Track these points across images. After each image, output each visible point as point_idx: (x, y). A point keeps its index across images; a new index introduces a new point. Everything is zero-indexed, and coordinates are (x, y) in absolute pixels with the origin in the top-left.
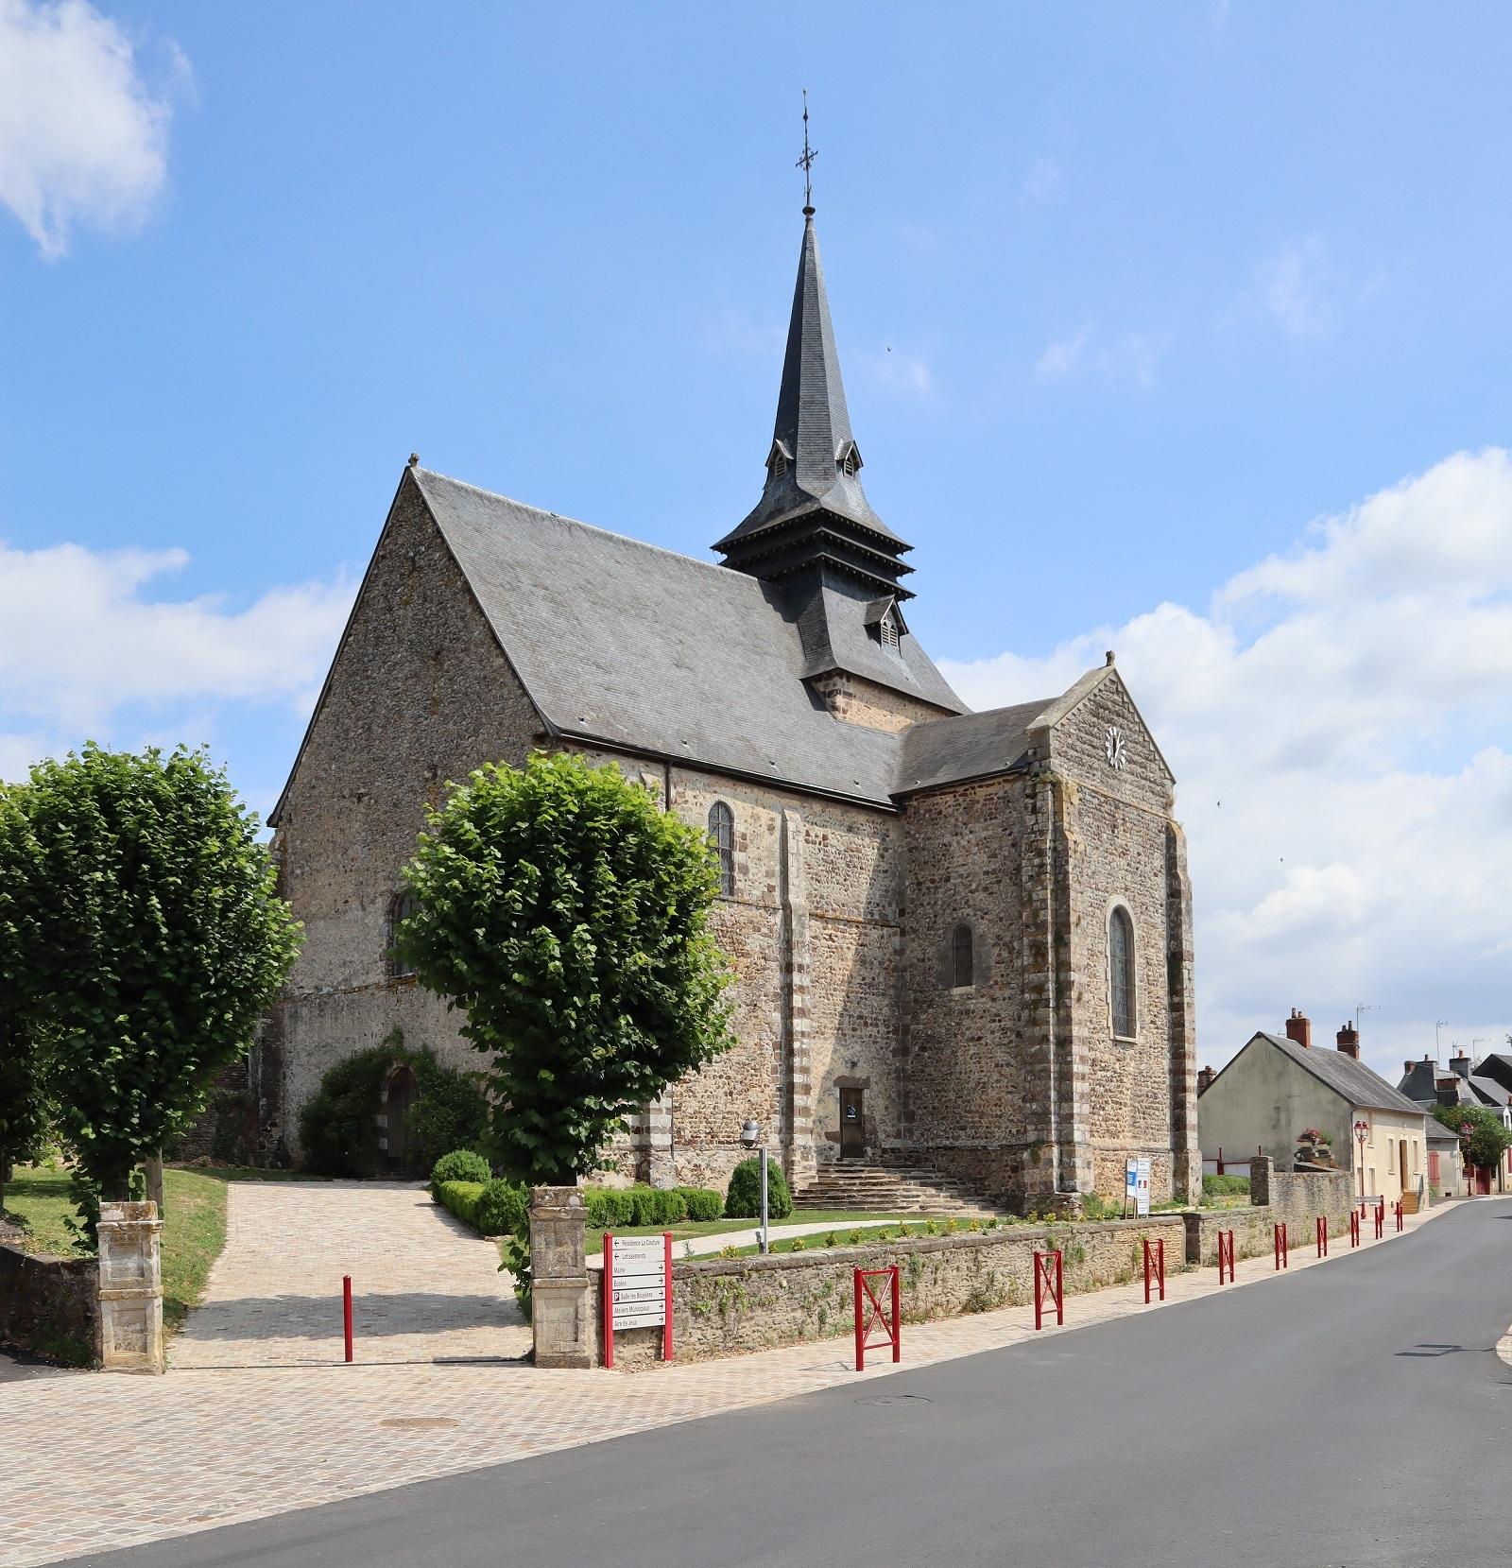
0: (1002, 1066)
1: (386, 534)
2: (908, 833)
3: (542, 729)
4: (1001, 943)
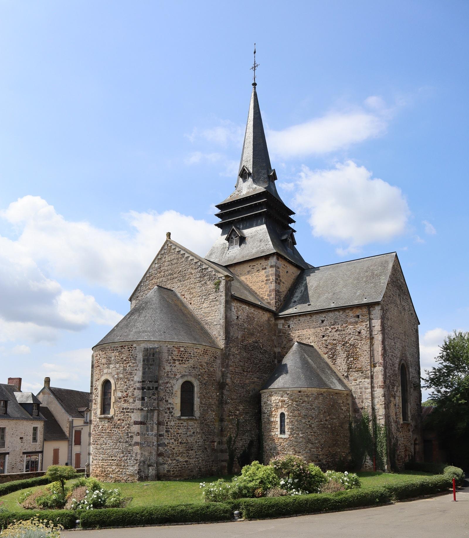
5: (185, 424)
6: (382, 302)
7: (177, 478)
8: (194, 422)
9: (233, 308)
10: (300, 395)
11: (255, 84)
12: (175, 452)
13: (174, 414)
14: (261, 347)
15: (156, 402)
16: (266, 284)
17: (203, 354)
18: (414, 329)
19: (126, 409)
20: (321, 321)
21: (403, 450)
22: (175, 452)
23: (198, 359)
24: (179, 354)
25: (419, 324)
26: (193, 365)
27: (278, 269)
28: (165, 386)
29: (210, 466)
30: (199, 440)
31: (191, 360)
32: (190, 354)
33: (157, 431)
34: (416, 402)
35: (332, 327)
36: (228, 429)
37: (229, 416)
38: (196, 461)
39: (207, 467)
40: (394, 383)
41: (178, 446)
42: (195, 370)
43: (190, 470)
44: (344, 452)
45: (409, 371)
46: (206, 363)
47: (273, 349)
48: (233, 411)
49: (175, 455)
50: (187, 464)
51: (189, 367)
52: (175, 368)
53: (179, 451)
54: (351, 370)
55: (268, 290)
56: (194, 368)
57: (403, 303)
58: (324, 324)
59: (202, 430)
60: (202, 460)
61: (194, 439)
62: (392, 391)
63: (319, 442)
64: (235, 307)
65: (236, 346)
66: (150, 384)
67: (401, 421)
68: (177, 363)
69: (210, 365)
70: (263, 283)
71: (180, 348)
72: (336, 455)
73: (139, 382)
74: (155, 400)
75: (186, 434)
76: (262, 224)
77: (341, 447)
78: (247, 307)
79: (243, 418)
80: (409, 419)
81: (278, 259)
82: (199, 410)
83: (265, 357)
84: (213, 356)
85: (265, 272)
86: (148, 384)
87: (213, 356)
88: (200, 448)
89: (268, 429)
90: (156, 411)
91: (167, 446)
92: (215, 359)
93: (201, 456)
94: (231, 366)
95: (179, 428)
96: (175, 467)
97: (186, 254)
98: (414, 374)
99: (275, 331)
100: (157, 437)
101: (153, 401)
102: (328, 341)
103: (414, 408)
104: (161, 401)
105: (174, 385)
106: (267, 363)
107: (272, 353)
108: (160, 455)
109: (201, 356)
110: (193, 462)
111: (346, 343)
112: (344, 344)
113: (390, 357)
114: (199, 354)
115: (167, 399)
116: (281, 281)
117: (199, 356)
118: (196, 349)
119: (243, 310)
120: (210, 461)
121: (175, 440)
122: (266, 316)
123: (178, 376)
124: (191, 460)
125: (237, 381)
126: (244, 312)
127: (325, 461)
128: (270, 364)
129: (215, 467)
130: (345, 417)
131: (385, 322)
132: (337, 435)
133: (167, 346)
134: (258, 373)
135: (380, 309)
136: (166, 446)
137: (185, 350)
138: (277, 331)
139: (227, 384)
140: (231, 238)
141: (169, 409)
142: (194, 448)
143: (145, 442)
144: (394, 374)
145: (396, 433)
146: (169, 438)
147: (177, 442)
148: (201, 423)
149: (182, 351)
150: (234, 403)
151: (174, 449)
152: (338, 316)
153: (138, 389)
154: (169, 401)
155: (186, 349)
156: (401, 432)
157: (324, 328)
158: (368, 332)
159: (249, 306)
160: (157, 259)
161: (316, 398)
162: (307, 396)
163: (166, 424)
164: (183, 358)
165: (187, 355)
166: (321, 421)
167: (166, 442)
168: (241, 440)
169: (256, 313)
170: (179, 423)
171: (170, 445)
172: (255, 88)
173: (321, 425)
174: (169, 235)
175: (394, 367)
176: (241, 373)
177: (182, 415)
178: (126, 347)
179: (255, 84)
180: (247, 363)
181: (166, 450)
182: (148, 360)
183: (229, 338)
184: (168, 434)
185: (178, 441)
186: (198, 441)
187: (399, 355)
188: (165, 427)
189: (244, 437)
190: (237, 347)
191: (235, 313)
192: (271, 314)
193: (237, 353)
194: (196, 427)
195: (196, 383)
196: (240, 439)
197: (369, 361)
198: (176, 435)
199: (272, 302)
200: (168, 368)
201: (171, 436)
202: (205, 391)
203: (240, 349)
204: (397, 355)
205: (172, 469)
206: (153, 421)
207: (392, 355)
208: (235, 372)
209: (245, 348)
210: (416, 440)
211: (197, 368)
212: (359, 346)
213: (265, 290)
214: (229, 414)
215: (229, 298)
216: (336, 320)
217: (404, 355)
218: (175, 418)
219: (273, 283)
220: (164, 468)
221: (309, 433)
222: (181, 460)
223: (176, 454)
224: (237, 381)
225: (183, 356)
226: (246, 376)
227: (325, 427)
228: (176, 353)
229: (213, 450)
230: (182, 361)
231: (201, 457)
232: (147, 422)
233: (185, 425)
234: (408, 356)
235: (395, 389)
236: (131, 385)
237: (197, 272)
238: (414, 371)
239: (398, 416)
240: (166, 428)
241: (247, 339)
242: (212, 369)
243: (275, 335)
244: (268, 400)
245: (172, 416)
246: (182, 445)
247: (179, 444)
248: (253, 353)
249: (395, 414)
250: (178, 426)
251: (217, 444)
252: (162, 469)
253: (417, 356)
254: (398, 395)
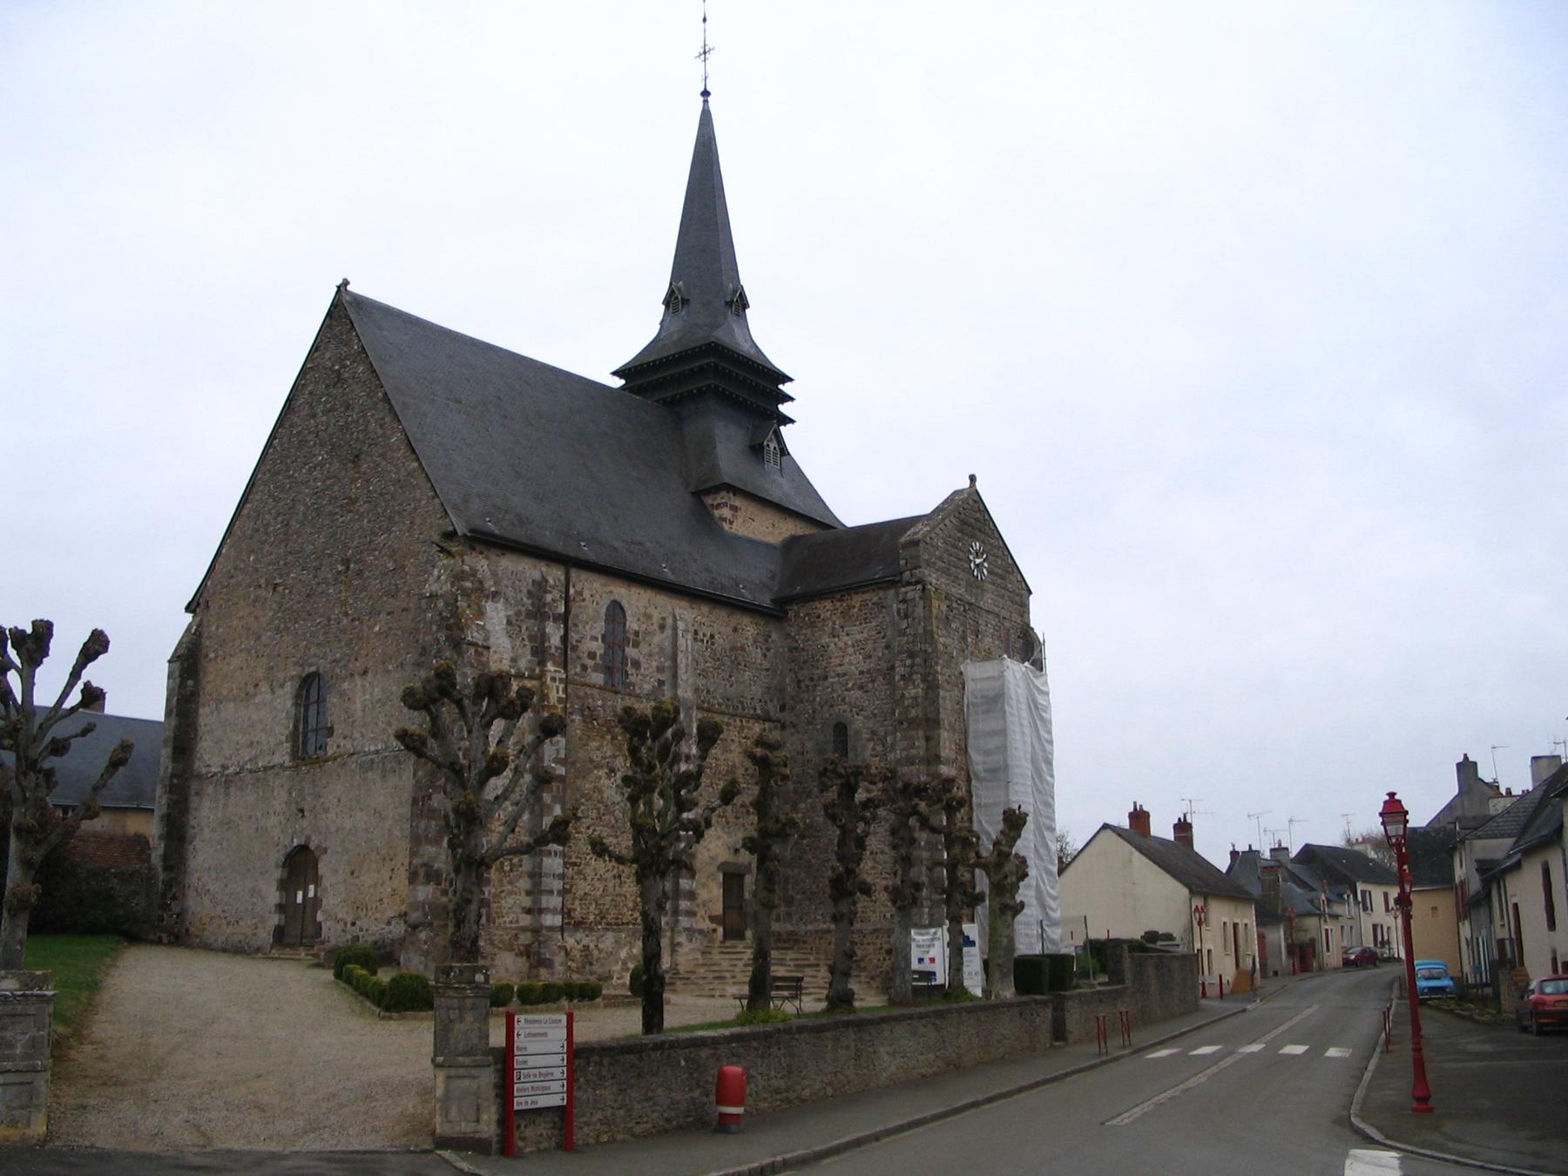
0: (877, 853)
1: (316, 347)
2: (789, 635)
3: (451, 529)
4: (875, 737)
11: (706, 93)
172: (706, 102)
179: (706, 93)
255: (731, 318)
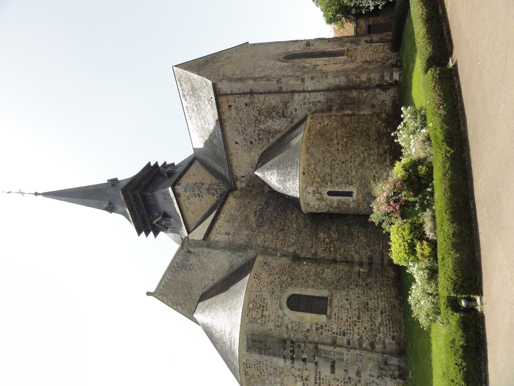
5: (336, 310)
6: (214, 81)
7: (402, 328)
8: (334, 297)
9: (216, 239)
10: (308, 173)
12: (370, 327)
13: (324, 323)
14: (261, 207)
15: (308, 345)
16: (202, 197)
17: (258, 279)
18: (251, 47)
19: (316, 380)
20: (237, 145)
21: (377, 54)
22: (370, 327)
23: (264, 287)
24: (257, 310)
25: (248, 43)
26: (270, 293)
27: (189, 185)
28: (291, 330)
29: (389, 281)
30: (355, 293)
31: (264, 295)
32: (257, 296)
33: (343, 347)
34: (326, 43)
35: (241, 133)
36: (346, 253)
37: (331, 252)
38: (382, 299)
39: (389, 285)
40: (301, 67)
41: (362, 322)
42: (275, 292)
43: (393, 308)
44: (377, 122)
45: (292, 52)
46: (269, 277)
47: (266, 194)
48: (325, 246)
49: (373, 327)
50: (386, 312)
51: (272, 299)
52: (271, 316)
53: (368, 321)
54: (285, 114)
55: (208, 195)
56: (273, 293)
57: (223, 59)
58: (239, 142)
59: (344, 288)
60: (381, 291)
61: (354, 299)
62: (309, 69)
63: (363, 152)
64: (215, 237)
65: (256, 238)
66: (287, 350)
67: (345, 57)
68: (265, 313)
69: (272, 271)
70: (202, 200)
71: (250, 308)
72: (380, 132)
73: (285, 361)
74: (306, 346)
75: (348, 309)
76: (153, 196)
77: (370, 126)
78: (219, 221)
79: (334, 233)
80: (342, 49)
81: (179, 184)
82: (321, 290)
83: (272, 203)
84: (263, 266)
85: (192, 197)
86: (287, 352)
87: (263, 266)
88: (366, 293)
89: (347, 209)
90: (320, 346)
91: (362, 336)
92: (266, 264)
93: (375, 292)
94: (276, 245)
95: (340, 318)
96: (388, 329)
97: (164, 280)
98: (296, 46)
99: (248, 190)
100: (351, 348)
101: (306, 349)
102: (256, 138)
103: (332, 45)
104: (307, 338)
105: (290, 319)
106: (278, 201)
107: (269, 195)
108: (372, 345)
109: (261, 283)
110: (383, 304)
111: (257, 118)
112: (258, 121)
113: (272, 72)
114: (259, 285)
115: (305, 330)
116: (200, 182)
117: (260, 285)
118: (252, 289)
119: (221, 227)
120: (382, 280)
121: (355, 325)
122: (231, 200)
123: (280, 313)
124: (380, 306)
125: (292, 239)
126: (222, 226)
127: (386, 146)
128: (281, 198)
129: (389, 274)
130: (336, 121)
131: (235, 78)
132: (356, 130)
133: (246, 323)
134: (288, 213)
135: (220, 83)
136: (361, 338)
137: (252, 302)
138: (248, 188)
139: (295, 251)
140: (165, 225)
141: (317, 329)
142: (366, 301)
143: (356, 365)
144: (292, 67)
145: (357, 63)
146: (352, 333)
147: (358, 324)
148: (336, 289)
149: (253, 306)
150: (316, 244)
151: (365, 328)
152: (230, 127)
153: (293, 363)
154: (309, 327)
155: (251, 301)
156: (356, 58)
157: (243, 141)
158: (245, 96)
159: (218, 219)
160: (173, 306)
161: (312, 155)
162: (309, 165)
163: (335, 335)
164: (260, 305)
165: (258, 301)
166: (338, 150)
167: (357, 337)
168: (358, 237)
169: (226, 212)
170: (335, 318)
171: (361, 333)
173: (343, 150)
174: (149, 294)
175: (284, 67)
176: (285, 233)
177: (325, 313)
178: (246, 369)
180: (275, 225)
181: (367, 338)
182: (260, 349)
183: (246, 246)
184: (348, 333)
185: (356, 321)
186: (357, 295)
187: (273, 62)
188: (338, 337)
189: (356, 234)
190: (257, 237)
191: (222, 237)
192: (230, 194)
193: (263, 237)
194: (341, 296)
195: (290, 291)
196: (357, 239)
197: (276, 94)
198: (349, 323)
199: (219, 193)
200: (271, 325)
201: (350, 330)
202: (300, 280)
203: (259, 232)
204: (273, 64)
205: (390, 332)
206: (330, 351)
207: (272, 69)
208: (283, 240)
209: (259, 226)
210: (366, 41)
211: (273, 289)
212: (260, 106)
213: (208, 199)
214: (328, 251)
215: (205, 243)
216: (235, 129)
217: (274, 57)
218: (328, 322)
219: (201, 191)
220: (390, 344)
221: (351, 164)
222: (380, 319)
223: (371, 325)
224: (293, 239)
225: (259, 305)
226: (289, 227)
227: (346, 145)
228: (254, 314)
229: (369, 274)
230: (264, 308)
231: (377, 292)
232: (331, 359)
233: (337, 311)
234: (276, 53)
235: (308, 65)
236: (288, 371)
237: (182, 271)
238: (293, 46)
239: (338, 61)
240: (340, 335)
241: (251, 224)
242: (277, 269)
243: (251, 191)
244: (314, 207)
245: (326, 326)
246: (361, 316)
247: (360, 321)
248: (266, 217)
249: (335, 65)
250: (338, 319)
251: (362, 267)
252: (391, 346)
253: (279, 44)
254: (315, 62)
255: (119, 184)
